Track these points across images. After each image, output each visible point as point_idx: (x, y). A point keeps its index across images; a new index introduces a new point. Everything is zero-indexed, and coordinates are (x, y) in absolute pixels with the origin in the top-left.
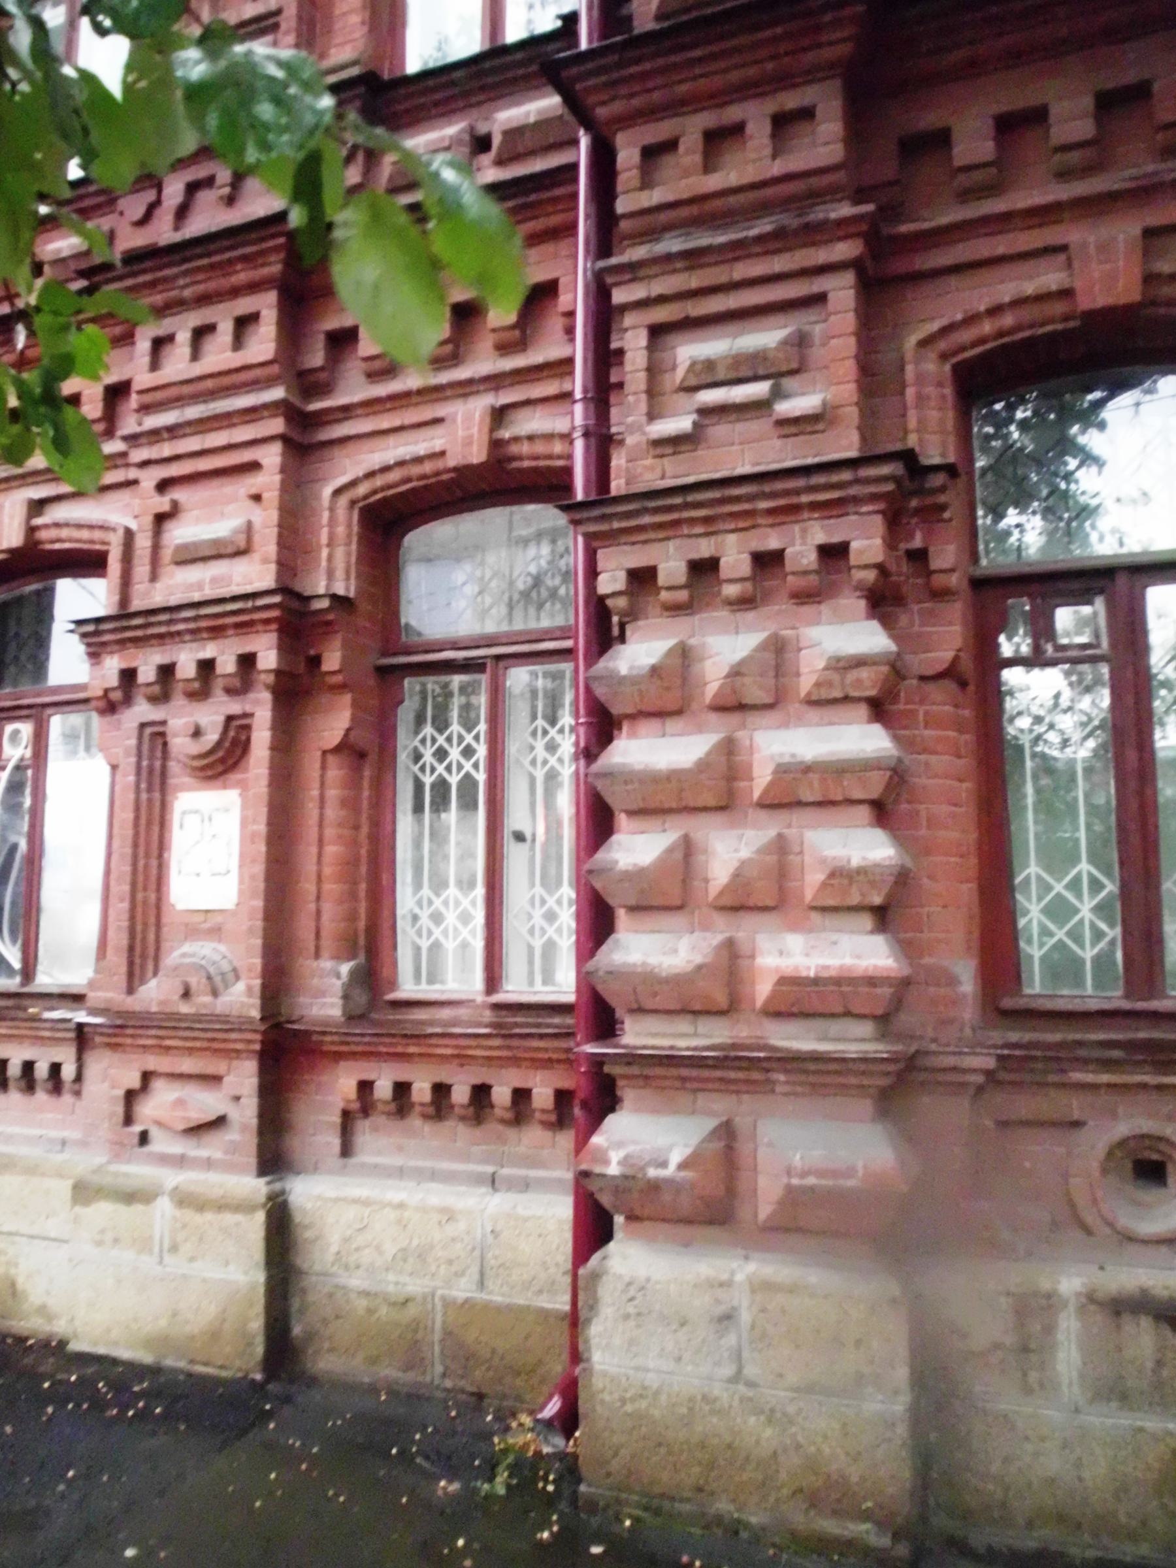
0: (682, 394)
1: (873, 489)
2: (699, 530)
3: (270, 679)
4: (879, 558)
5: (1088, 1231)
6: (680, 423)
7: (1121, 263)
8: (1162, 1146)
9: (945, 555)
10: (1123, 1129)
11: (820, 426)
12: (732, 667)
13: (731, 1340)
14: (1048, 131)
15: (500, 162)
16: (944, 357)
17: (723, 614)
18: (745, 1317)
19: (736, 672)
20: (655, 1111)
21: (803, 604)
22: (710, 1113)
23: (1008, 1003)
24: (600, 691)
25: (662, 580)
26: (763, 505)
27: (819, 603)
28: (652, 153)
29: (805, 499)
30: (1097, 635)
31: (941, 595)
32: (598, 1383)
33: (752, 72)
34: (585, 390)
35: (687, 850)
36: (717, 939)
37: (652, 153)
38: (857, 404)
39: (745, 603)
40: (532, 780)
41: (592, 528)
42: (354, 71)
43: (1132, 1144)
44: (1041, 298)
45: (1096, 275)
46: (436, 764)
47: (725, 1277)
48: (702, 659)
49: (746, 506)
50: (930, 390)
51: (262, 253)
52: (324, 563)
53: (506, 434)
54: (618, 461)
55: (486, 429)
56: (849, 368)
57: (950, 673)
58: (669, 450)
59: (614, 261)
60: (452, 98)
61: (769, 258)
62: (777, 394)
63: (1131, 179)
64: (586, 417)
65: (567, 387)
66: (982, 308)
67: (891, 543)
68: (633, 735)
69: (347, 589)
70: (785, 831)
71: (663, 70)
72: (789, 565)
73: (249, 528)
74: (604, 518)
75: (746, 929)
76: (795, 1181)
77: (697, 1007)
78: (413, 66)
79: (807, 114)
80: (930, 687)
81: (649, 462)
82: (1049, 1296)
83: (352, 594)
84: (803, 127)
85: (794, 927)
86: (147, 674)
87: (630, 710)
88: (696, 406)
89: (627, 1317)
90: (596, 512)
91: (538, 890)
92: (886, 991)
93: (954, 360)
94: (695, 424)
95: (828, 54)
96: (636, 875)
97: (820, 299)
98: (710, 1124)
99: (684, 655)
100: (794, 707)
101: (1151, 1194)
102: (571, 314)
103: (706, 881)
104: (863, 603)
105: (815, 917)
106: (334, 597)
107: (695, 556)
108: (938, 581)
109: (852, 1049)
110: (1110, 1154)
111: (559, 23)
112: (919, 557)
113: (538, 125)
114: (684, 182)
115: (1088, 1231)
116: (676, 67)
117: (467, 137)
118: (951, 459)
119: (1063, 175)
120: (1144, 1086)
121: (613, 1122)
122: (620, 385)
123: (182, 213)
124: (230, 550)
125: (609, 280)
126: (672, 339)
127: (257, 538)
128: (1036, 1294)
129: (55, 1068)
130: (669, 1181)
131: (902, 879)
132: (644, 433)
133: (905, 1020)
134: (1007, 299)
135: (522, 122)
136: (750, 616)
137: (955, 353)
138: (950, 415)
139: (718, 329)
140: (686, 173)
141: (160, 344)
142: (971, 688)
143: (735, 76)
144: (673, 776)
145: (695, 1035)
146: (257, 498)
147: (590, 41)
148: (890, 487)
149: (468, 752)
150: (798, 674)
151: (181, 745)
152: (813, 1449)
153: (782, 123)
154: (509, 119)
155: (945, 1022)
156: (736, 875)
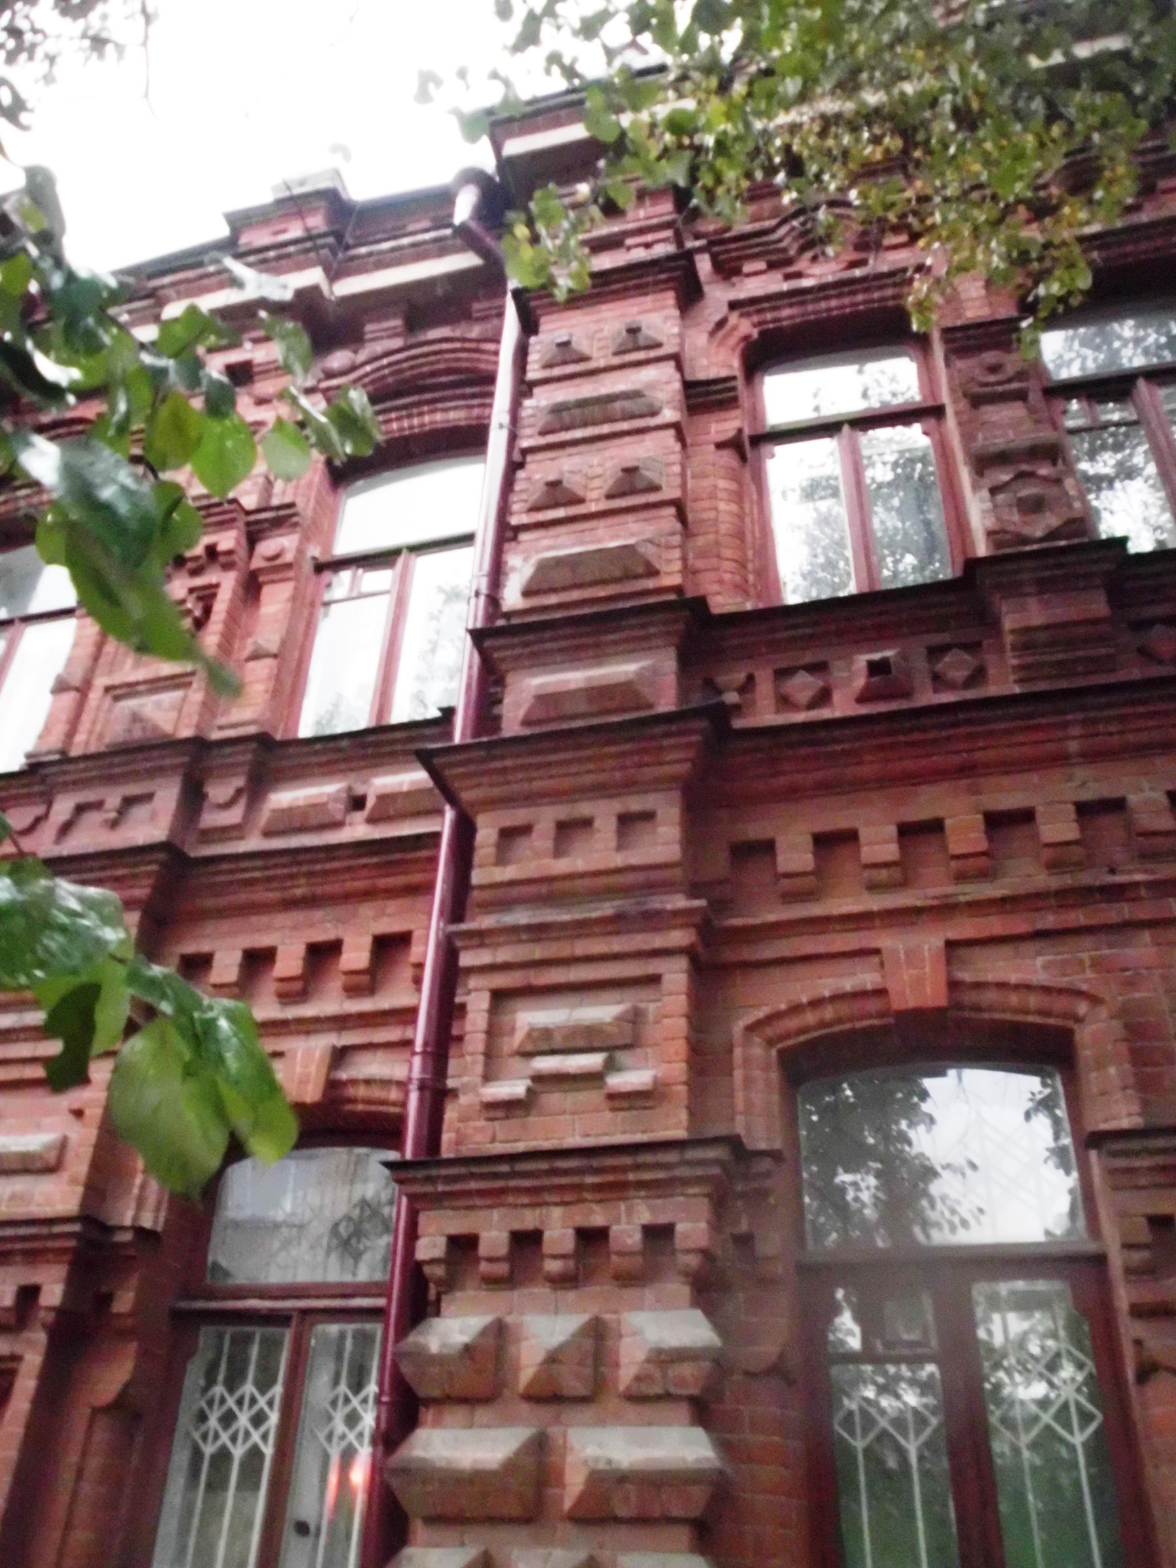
0: (517, 1058)
1: (699, 1172)
2: (525, 1200)
3: (50, 1317)
4: (703, 1242)
6: (513, 1088)
7: (927, 970)
11: (650, 1103)
12: (548, 1352)
14: (859, 851)
15: (372, 820)
16: (770, 1042)
17: (542, 1291)
19: (553, 1358)
21: (625, 1286)
24: (406, 1369)
25: (483, 1250)
26: (590, 1180)
27: (643, 1286)
28: (508, 835)
29: (631, 1177)
30: (925, 1332)
33: (602, 777)
34: (426, 1044)
37: (508, 835)
38: (685, 1083)
39: (565, 1281)
40: (326, 1458)
41: (417, 1189)
42: (252, 730)
44: (859, 995)
45: (906, 977)
46: (235, 1408)
48: (518, 1340)
49: (576, 1180)
50: (757, 1073)
51: (135, 876)
52: (136, 1191)
53: (343, 1075)
54: (451, 1114)
55: (324, 1070)
56: (679, 1047)
57: (776, 1370)
58: (500, 1114)
59: (464, 927)
60: (336, 762)
61: (609, 938)
62: (611, 1066)
63: (934, 898)
64: (424, 1069)
65: (409, 1034)
66: (805, 1000)
68: (437, 1423)
69: (156, 1221)
70: (595, 1553)
71: (523, 768)
72: (613, 1244)
73: (63, 1145)
74: (429, 1180)
78: (306, 729)
79: (648, 816)
83: (159, 1228)
87: (436, 1393)
88: (531, 1072)
90: (420, 1174)
93: (780, 1046)
94: (529, 1090)
95: (667, 770)
97: (654, 980)
99: (499, 1333)
100: (612, 1403)
102: (420, 966)
104: (686, 1290)
106: (140, 1231)
107: (517, 1226)
111: (438, 714)
112: (744, 1241)
113: (408, 794)
116: (538, 767)
117: (344, 795)
118: (777, 1145)
119: (873, 887)
122: (460, 1039)
123: (66, 829)
124: (39, 1165)
125: (459, 943)
127: (70, 1156)
132: (479, 1095)
134: (827, 993)
135: (397, 789)
136: (571, 1295)
138: (775, 1098)
139: (555, 1000)
140: (538, 855)
143: (588, 779)
144: (477, 1479)
146: (78, 1114)
147: (463, 735)
148: (716, 1170)
149: (258, 1419)
150: (617, 1365)
153: (626, 821)
154: (385, 786)
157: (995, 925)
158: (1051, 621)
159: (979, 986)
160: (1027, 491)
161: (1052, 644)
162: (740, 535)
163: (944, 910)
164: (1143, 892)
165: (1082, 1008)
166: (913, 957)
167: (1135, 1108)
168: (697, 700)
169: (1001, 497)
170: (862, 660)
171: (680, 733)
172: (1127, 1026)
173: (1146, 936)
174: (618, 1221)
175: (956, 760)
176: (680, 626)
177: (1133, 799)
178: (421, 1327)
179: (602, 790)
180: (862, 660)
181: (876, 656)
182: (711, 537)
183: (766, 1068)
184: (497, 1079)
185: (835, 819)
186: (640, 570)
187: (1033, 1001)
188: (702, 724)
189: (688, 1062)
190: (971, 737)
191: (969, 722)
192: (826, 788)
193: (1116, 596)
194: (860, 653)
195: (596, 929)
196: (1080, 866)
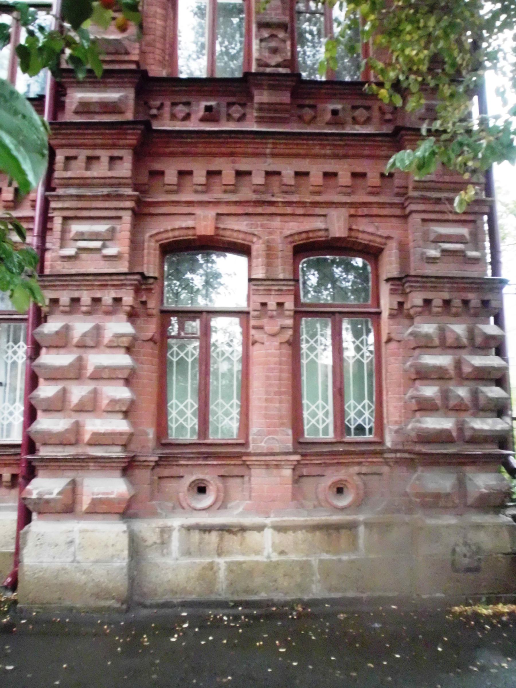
2: (75, 288)
4: (131, 304)
5: (183, 508)
6: (70, 251)
8: (205, 482)
9: (152, 304)
10: (194, 478)
13: (72, 549)
17: (81, 316)
18: (77, 541)
19: (84, 335)
20: (49, 477)
22: (68, 477)
23: (164, 441)
24: (37, 338)
26: (97, 283)
31: (150, 315)
32: (25, 569)
34: (38, 233)
35: (64, 391)
36: (73, 421)
37: (68, 159)
39: (88, 313)
43: (197, 482)
44: (188, 228)
47: (71, 529)
50: (152, 251)
56: (127, 242)
57: (151, 340)
62: (104, 246)
64: (38, 242)
67: (135, 299)
75: (82, 418)
76: (95, 497)
77: (65, 443)
80: (146, 344)
81: (59, 262)
82: (170, 527)
84: (118, 162)
85: (98, 417)
89: (36, 545)
92: (125, 437)
94: (77, 253)
95: (128, 142)
96: (48, 399)
97: (119, 218)
98: (68, 480)
99: (67, 328)
100: (102, 348)
101: (201, 496)
102: (34, 201)
103: (70, 402)
105: (105, 414)
108: (150, 311)
109: (114, 455)
110: (190, 486)
112: (144, 303)
114: (78, 172)
115: (183, 508)
118: (156, 275)
119: (196, 192)
120: (200, 465)
121: (35, 482)
125: (50, 199)
126: (70, 222)
128: (167, 527)
130: (54, 500)
131: (132, 402)
133: (132, 447)
137: (161, 240)
140: (80, 168)
142: (158, 344)
145: (64, 452)
148: (136, 282)
150: (103, 337)
152: (97, 580)
153: (112, 159)
155: (143, 447)
156: (80, 401)
157: (233, 209)
158: (270, 102)
159: (224, 229)
160: (273, 44)
161: (269, 110)
162: (164, 37)
163: (217, 203)
164: (280, 204)
165: (255, 239)
166: (205, 218)
167: (264, 271)
168: (142, 117)
169: (263, 44)
170: (204, 104)
171: (133, 129)
172: (268, 246)
173: (279, 218)
174: (104, 296)
175: (230, 150)
176: (136, 81)
177: (284, 172)
178: (41, 326)
179: (103, 146)
180: (204, 104)
181: (209, 104)
182: (152, 37)
183: (154, 265)
184: (65, 248)
185: (185, 166)
186: (123, 51)
187: (241, 236)
188: (142, 127)
189: (130, 247)
190: (235, 143)
191: (235, 138)
192: (185, 154)
193: (294, 95)
194: (203, 101)
195: (100, 199)
196: (263, 193)
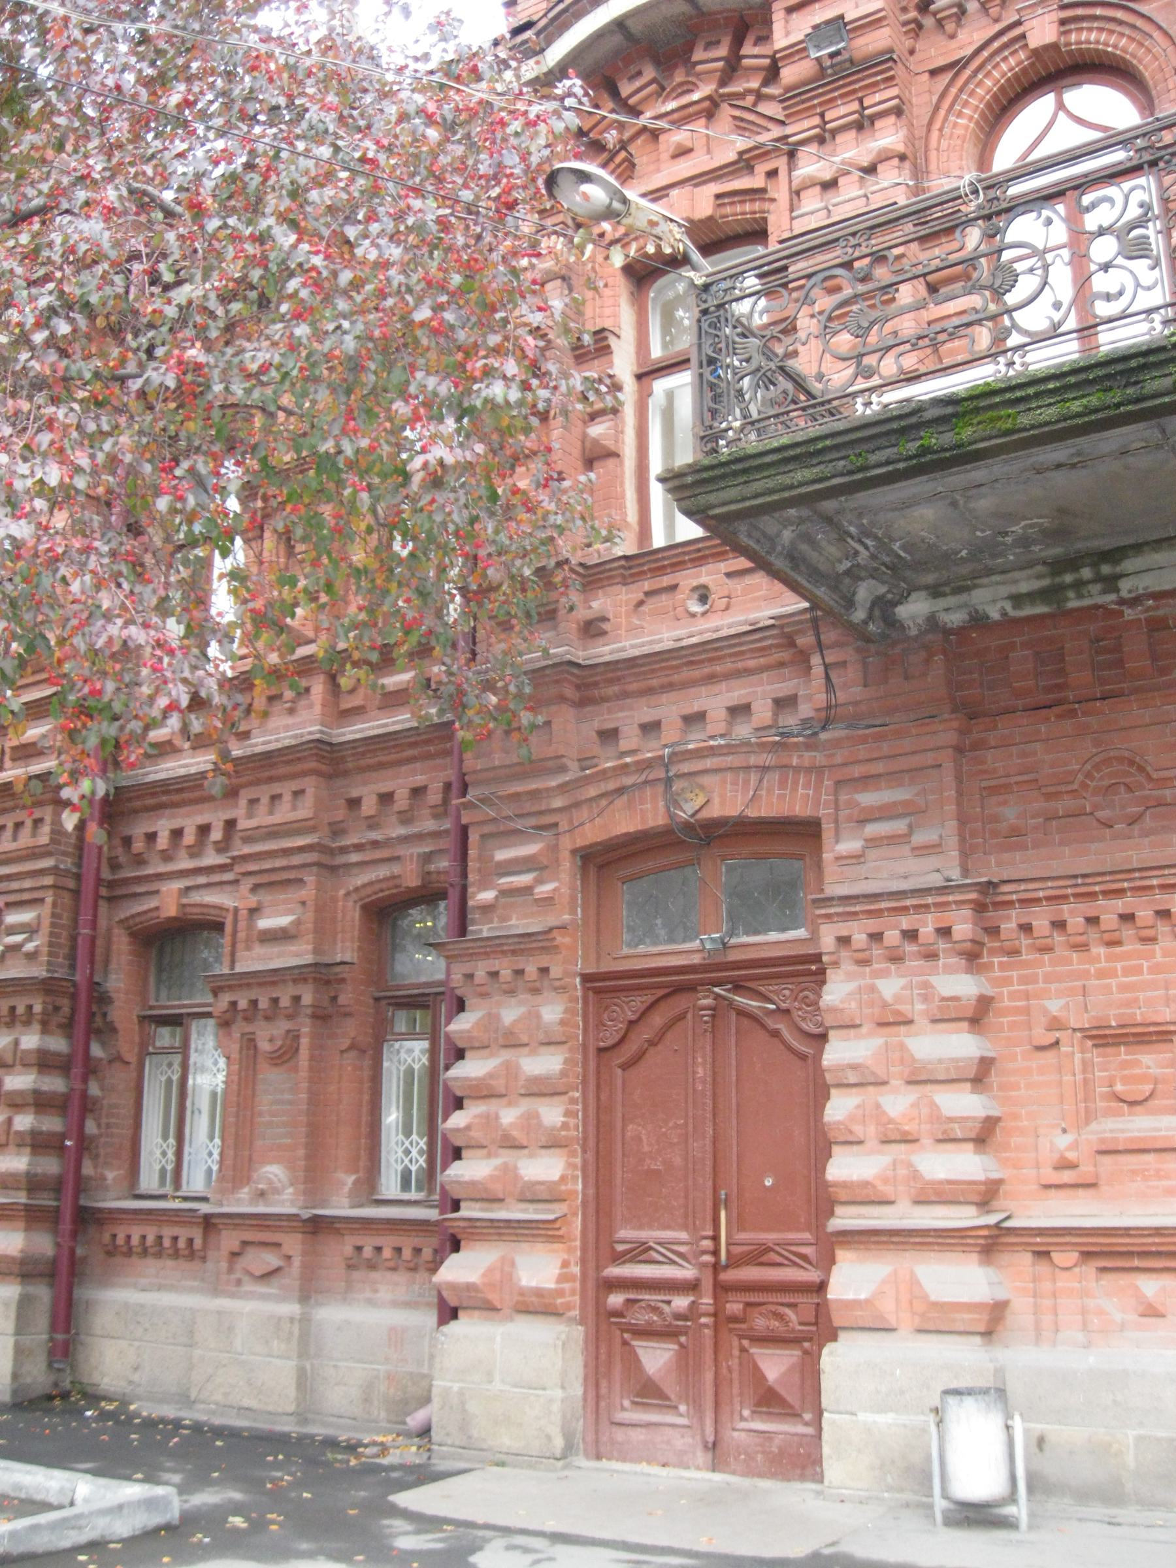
86: (243, 1004)
91: (401, 1137)
129: (190, 1241)
141: (253, 802)
151: (264, 1046)
